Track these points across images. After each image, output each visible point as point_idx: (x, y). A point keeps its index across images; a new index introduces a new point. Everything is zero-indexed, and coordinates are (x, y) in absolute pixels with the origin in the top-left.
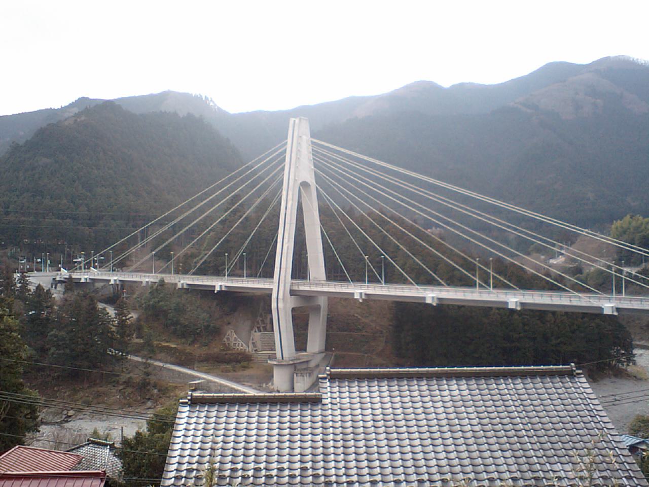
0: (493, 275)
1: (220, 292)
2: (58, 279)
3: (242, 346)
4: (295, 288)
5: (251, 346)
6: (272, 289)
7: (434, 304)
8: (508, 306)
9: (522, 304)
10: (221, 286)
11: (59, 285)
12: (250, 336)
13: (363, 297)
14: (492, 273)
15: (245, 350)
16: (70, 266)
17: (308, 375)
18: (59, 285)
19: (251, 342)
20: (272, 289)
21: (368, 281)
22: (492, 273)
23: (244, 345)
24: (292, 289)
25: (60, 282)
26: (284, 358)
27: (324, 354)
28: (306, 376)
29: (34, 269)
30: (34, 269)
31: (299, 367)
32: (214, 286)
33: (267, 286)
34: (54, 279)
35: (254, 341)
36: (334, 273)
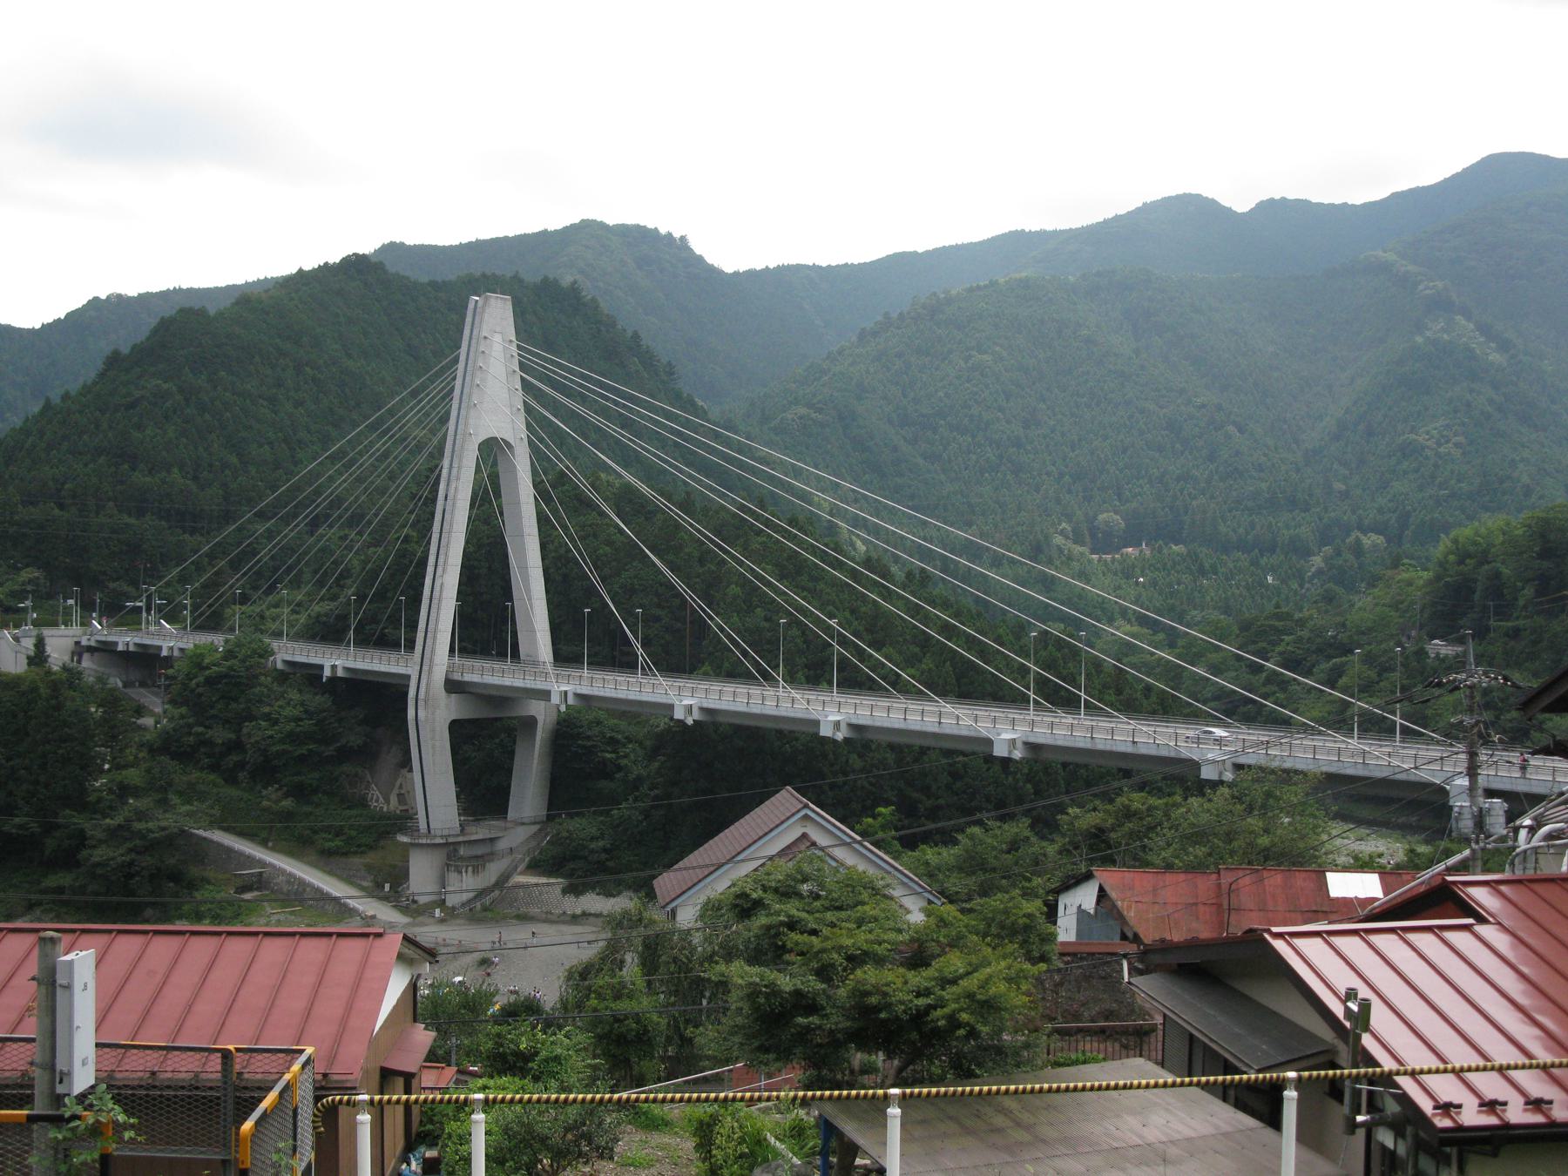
0: (1085, 699)
1: (334, 679)
2: (84, 642)
3: (377, 801)
4: (457, 677)
5: (394, 799)
6: (408, 677)
7: (690, 721)
8: (995, 750)
9: (1032, 747)
10: (334, 667)
11: (86, 656)
12: (396, 780)
13: (571, 701)
14: (1032, 696)
15: (382, 808)
16: (116, 612)
17: (470, 869)
18: (86, 656)
19: (396, 791)
20: (408, 677)
21: (386, 642)
22: (1032, 696)
23: (381, 799)
24: (450, 677)
25: (90, 649)
26: (432, 832)
27: (537, 827)
28: (466, 872)
29: (60, 622)
30: (60, 622)
31: (462, 851)
32: (321, 667)
33: (401, 670)
34: (77, 643)
35: (402, 792)
36: (565, 656)
